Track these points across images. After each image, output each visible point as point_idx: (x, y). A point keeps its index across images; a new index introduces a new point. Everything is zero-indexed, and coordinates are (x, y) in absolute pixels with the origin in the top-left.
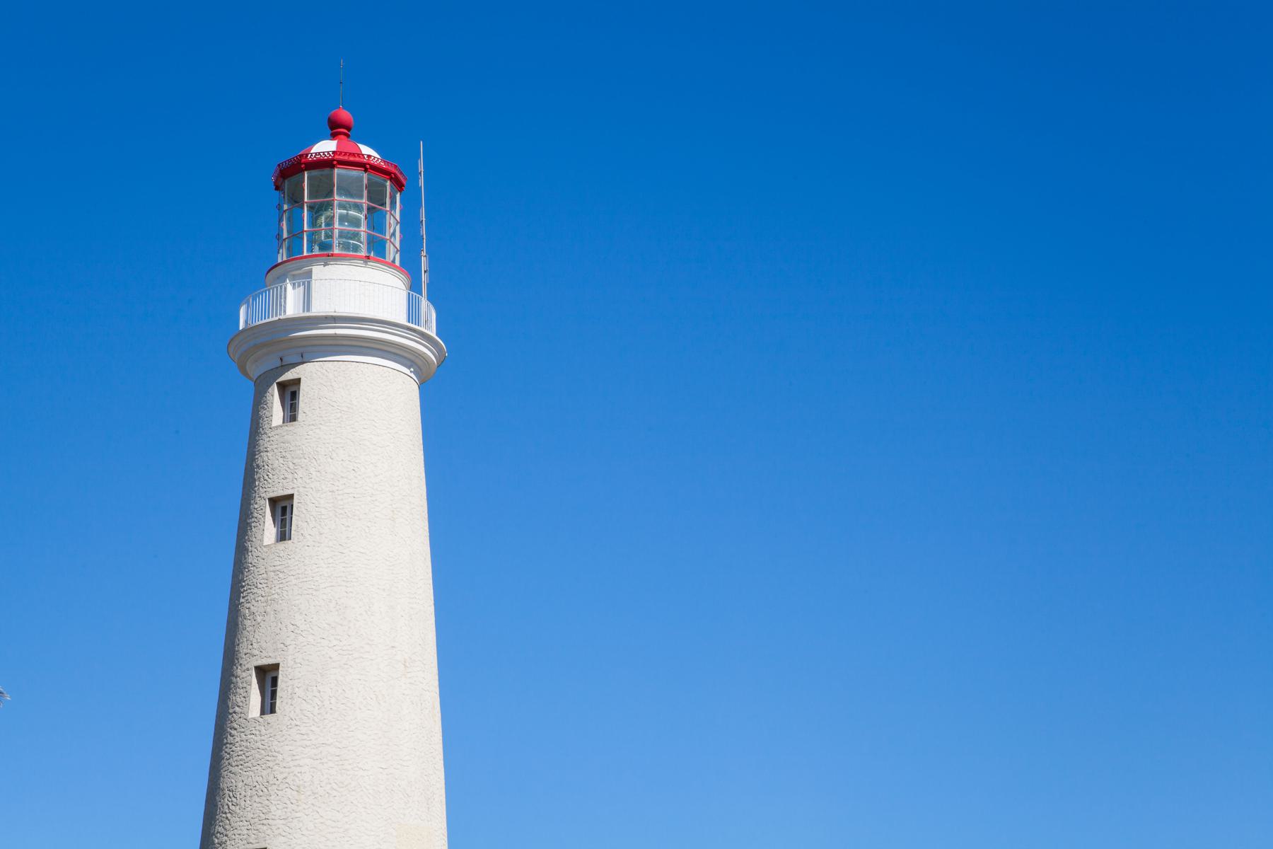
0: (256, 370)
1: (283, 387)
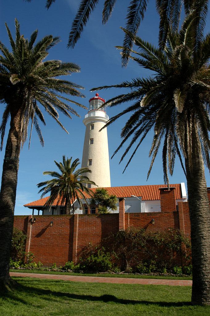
0: (87, 124)
1: (91, 125)
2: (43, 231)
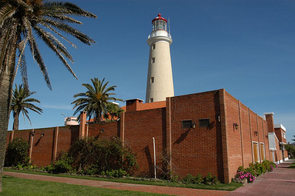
0: (150, 44)
1: (153, 45)
2: (39, 140)
